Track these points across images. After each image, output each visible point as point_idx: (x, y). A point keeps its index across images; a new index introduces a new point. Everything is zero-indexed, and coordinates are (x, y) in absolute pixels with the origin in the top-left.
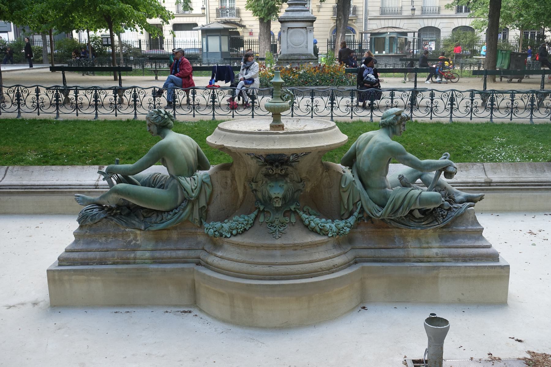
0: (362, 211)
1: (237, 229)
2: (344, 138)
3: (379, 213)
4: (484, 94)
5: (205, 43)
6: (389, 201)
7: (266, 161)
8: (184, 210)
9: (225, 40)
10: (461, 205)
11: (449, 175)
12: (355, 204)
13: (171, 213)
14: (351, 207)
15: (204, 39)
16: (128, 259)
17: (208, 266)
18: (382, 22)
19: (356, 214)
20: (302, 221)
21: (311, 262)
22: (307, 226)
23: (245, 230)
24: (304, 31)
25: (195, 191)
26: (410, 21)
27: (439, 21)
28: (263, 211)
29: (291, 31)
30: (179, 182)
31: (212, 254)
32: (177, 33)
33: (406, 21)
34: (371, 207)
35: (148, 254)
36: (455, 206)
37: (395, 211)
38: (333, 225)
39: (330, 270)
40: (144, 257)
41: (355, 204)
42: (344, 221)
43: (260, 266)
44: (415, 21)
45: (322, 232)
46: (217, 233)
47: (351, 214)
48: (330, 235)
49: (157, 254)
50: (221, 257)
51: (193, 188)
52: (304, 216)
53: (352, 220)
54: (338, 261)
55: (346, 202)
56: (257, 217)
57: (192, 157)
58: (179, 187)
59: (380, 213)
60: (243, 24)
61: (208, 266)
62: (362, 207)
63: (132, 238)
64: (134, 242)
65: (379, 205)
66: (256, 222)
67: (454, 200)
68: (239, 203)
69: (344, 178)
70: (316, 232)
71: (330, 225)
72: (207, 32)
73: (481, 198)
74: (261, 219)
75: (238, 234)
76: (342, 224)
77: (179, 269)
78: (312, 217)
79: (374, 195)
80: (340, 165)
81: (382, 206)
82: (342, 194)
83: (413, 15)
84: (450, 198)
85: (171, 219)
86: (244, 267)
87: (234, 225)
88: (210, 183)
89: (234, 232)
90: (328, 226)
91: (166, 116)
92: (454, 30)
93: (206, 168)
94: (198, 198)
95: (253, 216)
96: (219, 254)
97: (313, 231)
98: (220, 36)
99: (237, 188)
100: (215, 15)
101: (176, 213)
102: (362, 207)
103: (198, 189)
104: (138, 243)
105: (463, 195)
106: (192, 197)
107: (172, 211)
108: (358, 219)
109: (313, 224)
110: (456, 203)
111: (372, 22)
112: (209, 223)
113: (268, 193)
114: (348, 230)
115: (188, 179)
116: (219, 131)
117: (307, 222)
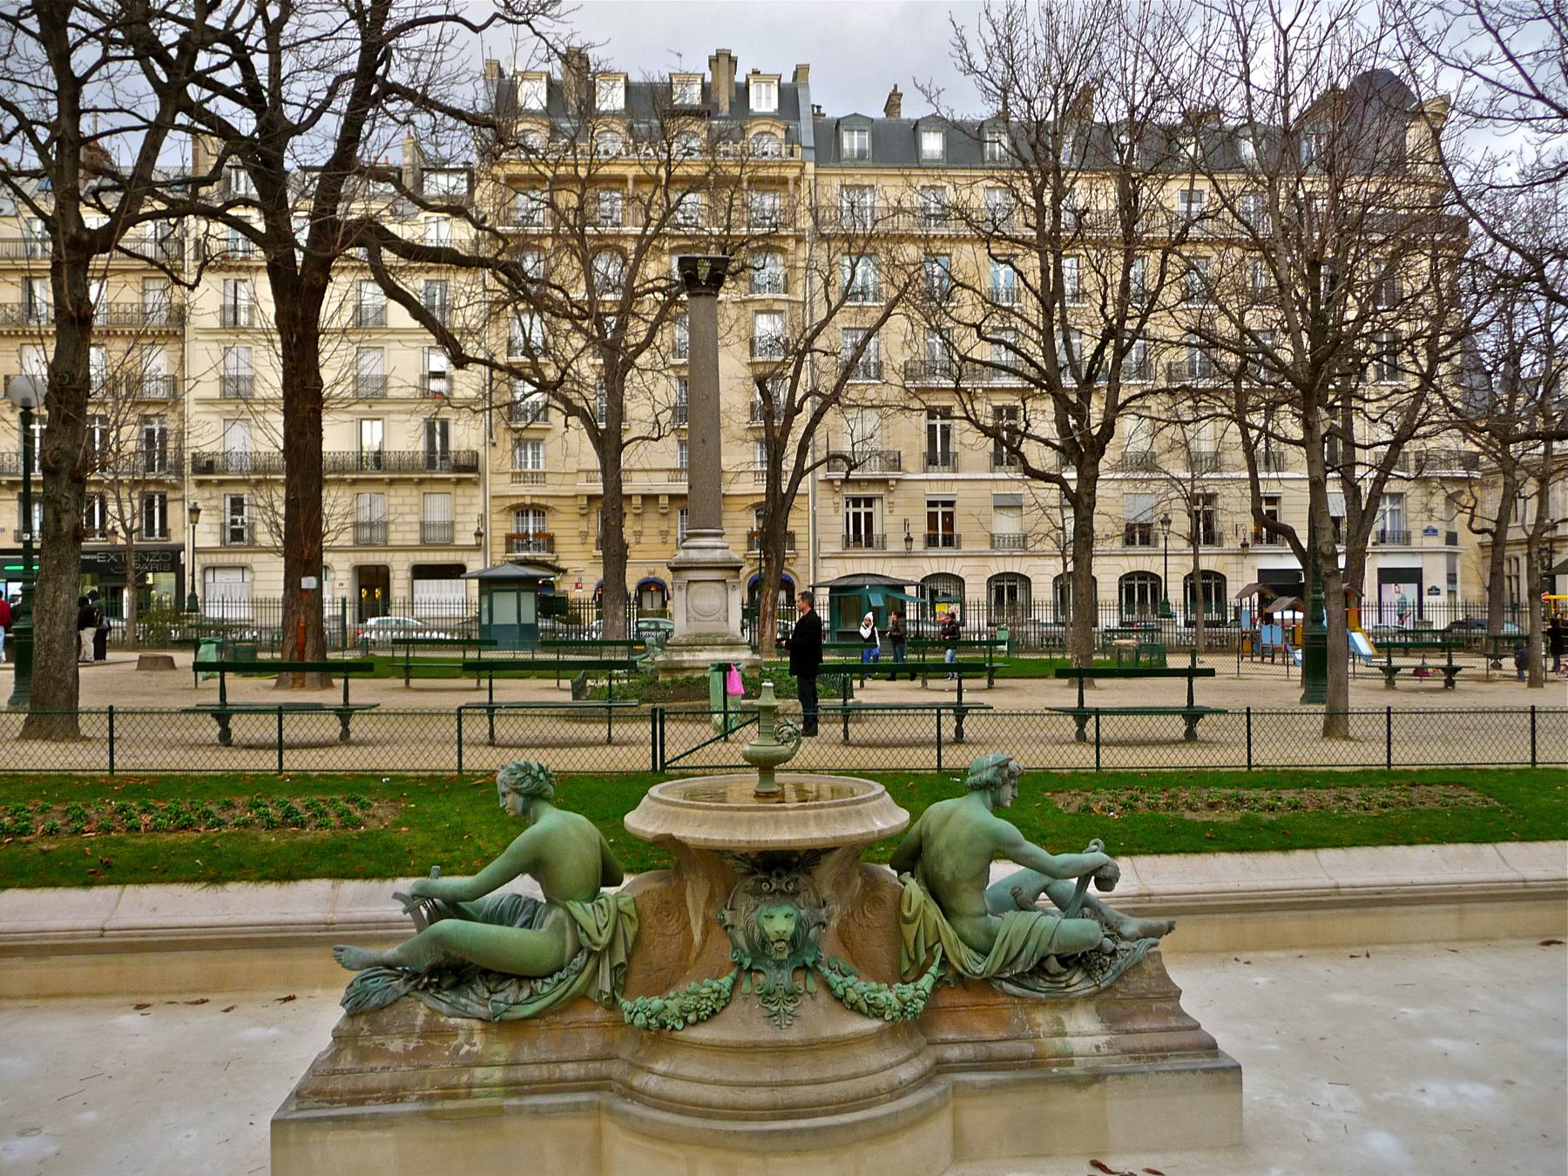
0: (945, 963)
1: (697, 1010)
2: (903, 816)
3: (979, 967)
4: (1081, 714)
5: (485, 606)
6: (998, 941)
7: (754, 863)
8: (579, 972)
9: (529, 601)
10: (1134, 945)
11: (1106, 883)
12: (929, 950)
13: (548, 980)
14: (923, 957)
15: (485, 599)
16: (456, 1087)
17: (632, 1093)
18: (849, 563)
19: (933, 970)
20: (828, 987)
21: (855, 1076)
22: (839, 1000)
23: (714, 1011)
24: (719, 586)
25: (604, 932)
26: (904, 562)
27: (960, 562)
28: (750, 970)
29: (694, 587)
30: (571, 915)
31: (642, 1068)
32: (420, 584)
33: (894, 562)
34: (963, 956)
35: (497, 1074)
36: (1123, 945)
37: (1009, 962)
38: (892, 996)
39: (897, 1092)
40: (490, 1081)
41: (929, 950)
42: (911, 986)
43: (754, 1090)
44: (913, 562)
45: (875, 1011)
46: (653, 1021)
47: (923, 971)
48: (888, 1017)
49: (519, 1074)
50: (665, 1075)
51: (601, 925)
52: (835, 978)
53: (926, 982)
54: (906, 1073)
55: (911, 943)
56: (736, 983)
57: (592, 859)
58: (567, 924)
59: (982, 967)
60: (563, 565)
61: (632, 1093)
62: (944, 954)
63: (461, 1039)
64: (466, 1048)
65: (976, 951)
66: (737, 993)
67: (1119, 934)
68: (693, 955)
69: (906, 899)
70: (860, 1012)
71: (887, 995)
72: (490, 584)
73: (1170, 928)
74: (746, 986)
75: (699, 1021)
76: (908, 991)
77: (568, 1104)
78: (850, 980)
79: (967, 928)
80: (887, 868)
81: (985, 953)
82: (904, 926)
83: (909, 550)
84: (1112, 928)
85: (547, 995)
86: (716, 1095)
87: (690, 1002)
88: (634, 915)
89: (692, 1018)
90: (882, 996)
91: (542, 776)
92: (1056, 579)
93: (617, 882)
94: (611, 946)
95: (727, 981)
96: (660, 1067)
97: (855, 1008)
98: (519, 592)
99: (689, 922)
100: (503, 548)
101: (560, 981)
102: (944, 954)
103: (610, 927)
104: (475, 1049)
105: (1132, 926)
106: (596, 945)
107: (551, 976)
108: (939, 980)
109: (852, 996)
110: (1123, 938)
111: (827, 563)
112: (632, 999)
113: (762, 929)
114: (921, 1004)
115: (588, 906)
116: (652, 803)
117: (840, 991)
